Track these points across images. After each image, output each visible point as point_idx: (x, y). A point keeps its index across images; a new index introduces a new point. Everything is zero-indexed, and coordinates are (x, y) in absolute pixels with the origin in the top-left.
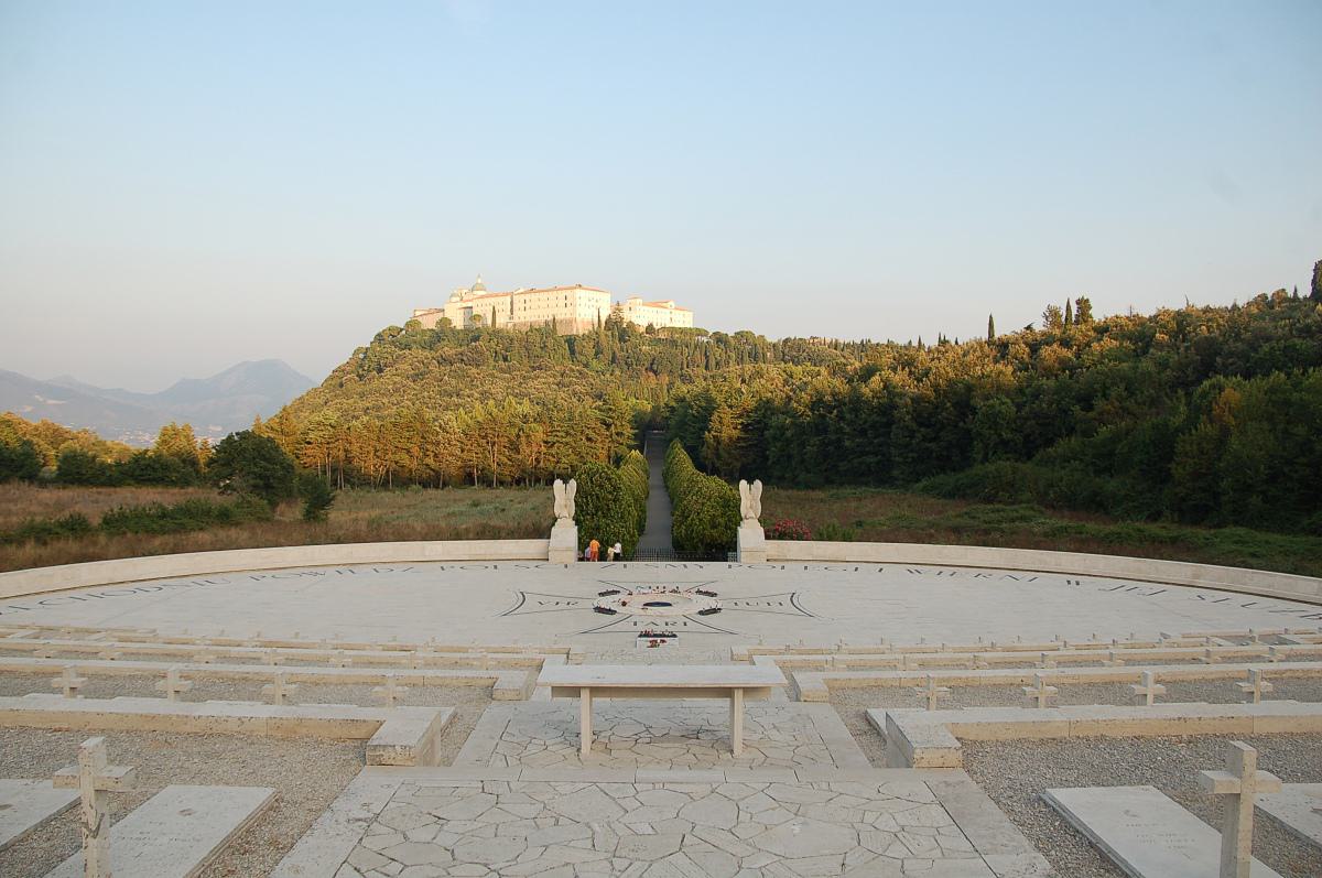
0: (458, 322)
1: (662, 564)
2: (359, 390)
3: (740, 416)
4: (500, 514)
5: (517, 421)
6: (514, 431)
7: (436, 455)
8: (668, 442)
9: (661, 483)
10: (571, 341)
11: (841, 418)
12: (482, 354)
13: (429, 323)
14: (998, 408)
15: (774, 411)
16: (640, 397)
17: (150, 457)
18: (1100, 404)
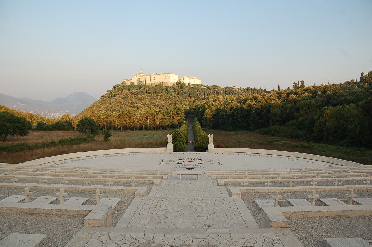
0: (136, 83)
1: (191, 153)
2: (109, 102)
3: (212, 112)
4: (151, 138)
7: (133, 122)
8: (193, 118)
9: (192, 129)
10: (167, 88)
12: (143, 92)
13: (128, 83)
14: (276, 112)
15: (221, 111)
16: (185, 105)
17: (60, 123)
18: (301, 111)
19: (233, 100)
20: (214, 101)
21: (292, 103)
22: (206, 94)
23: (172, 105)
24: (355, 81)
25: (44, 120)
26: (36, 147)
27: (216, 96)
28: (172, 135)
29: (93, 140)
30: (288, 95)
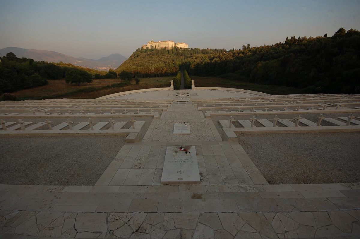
0: (150, 48)
5: (162, 67)
10: (168, 51)
13: (145, 48)
16: (179, 62)
19: (206, 58)
20: (195, 59)
21: (240, 59)
22: (191, 54)
23: (172, 61)
24: (282, 43)
25: (97, 72)
27: (197, 55)
28: (173, 81)
29: (130, 84)
30: (239, 54)
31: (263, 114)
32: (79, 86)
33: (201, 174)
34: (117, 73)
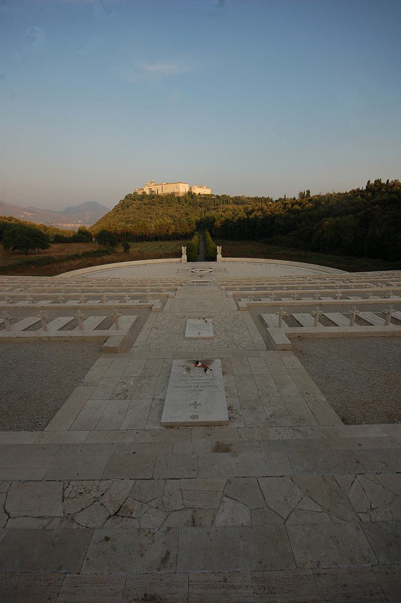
0: (148, 193)
5: (168, 224)
6: (167, 227)
10: (178, 198)
11: (244, 224)
12: (155, 202)
13: (140, 193)
16: (195, 217)
19: (241, 211)
23: (184, 215)
24: (361, 189)
25: (59, 232)
26: (61, 260)
27: (226, 206)
30: (293, 205)
31: (333, 304)
32: (26, 255)
33: (230, 408)
34: (93, 234)
